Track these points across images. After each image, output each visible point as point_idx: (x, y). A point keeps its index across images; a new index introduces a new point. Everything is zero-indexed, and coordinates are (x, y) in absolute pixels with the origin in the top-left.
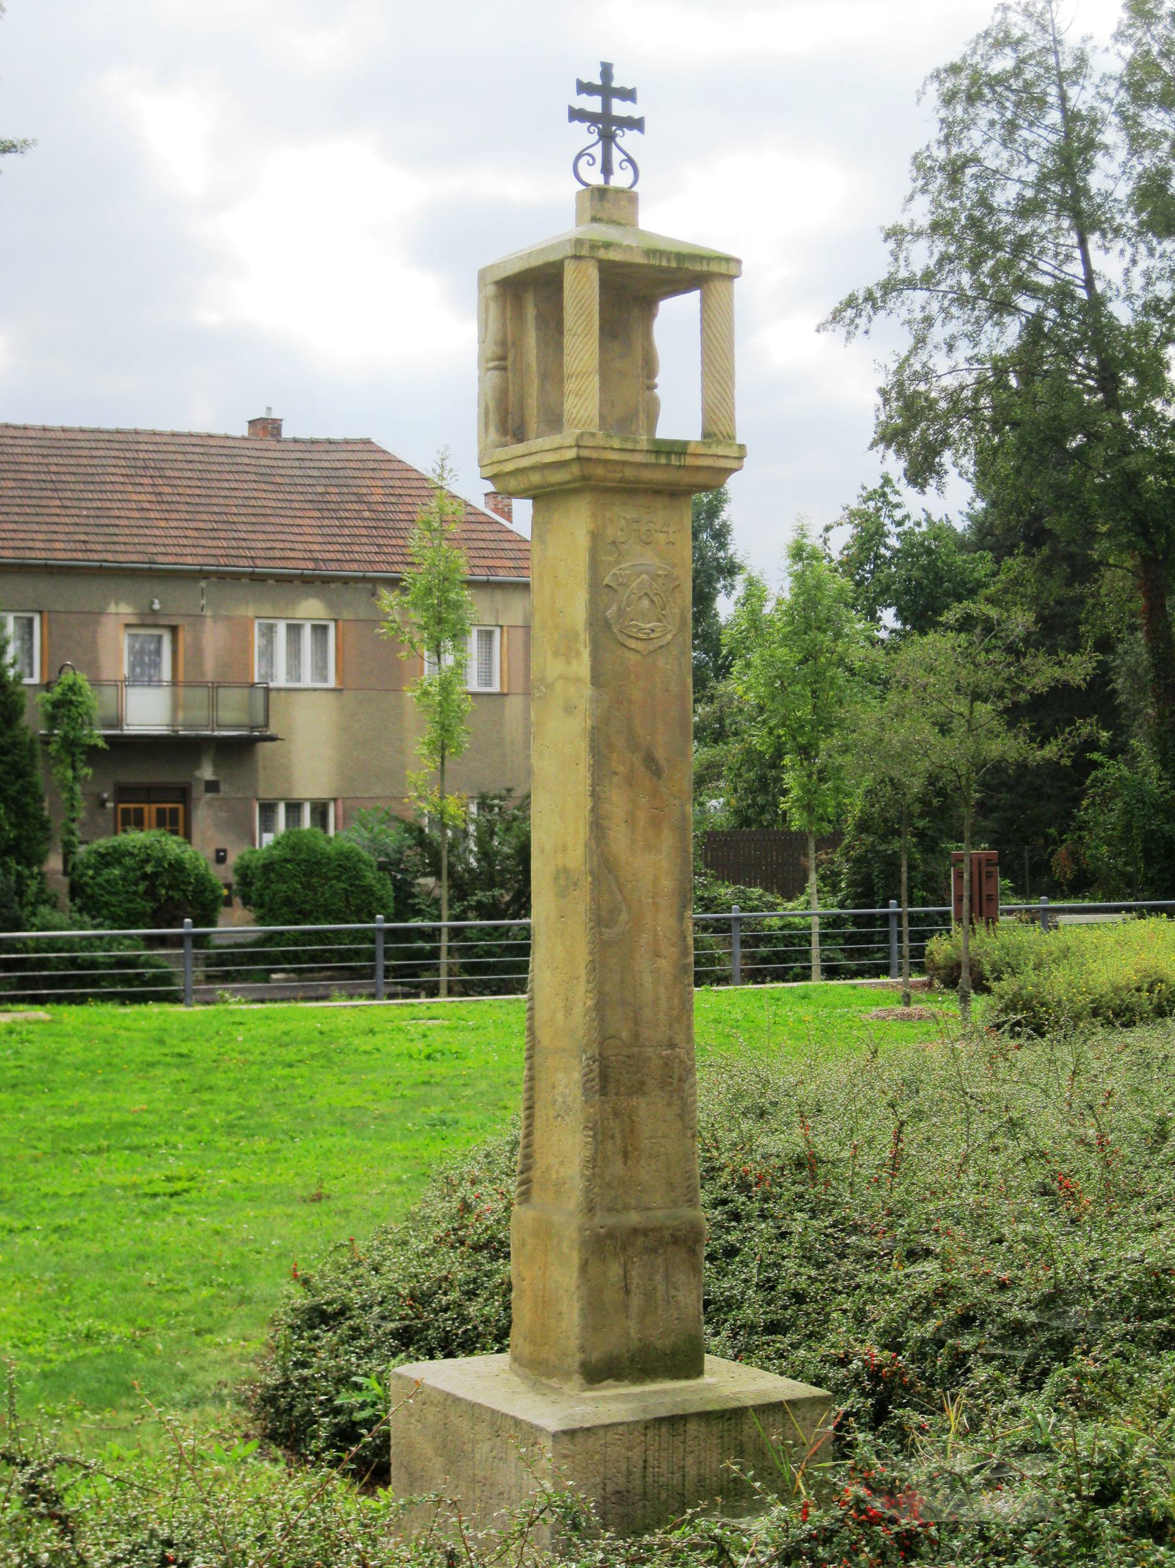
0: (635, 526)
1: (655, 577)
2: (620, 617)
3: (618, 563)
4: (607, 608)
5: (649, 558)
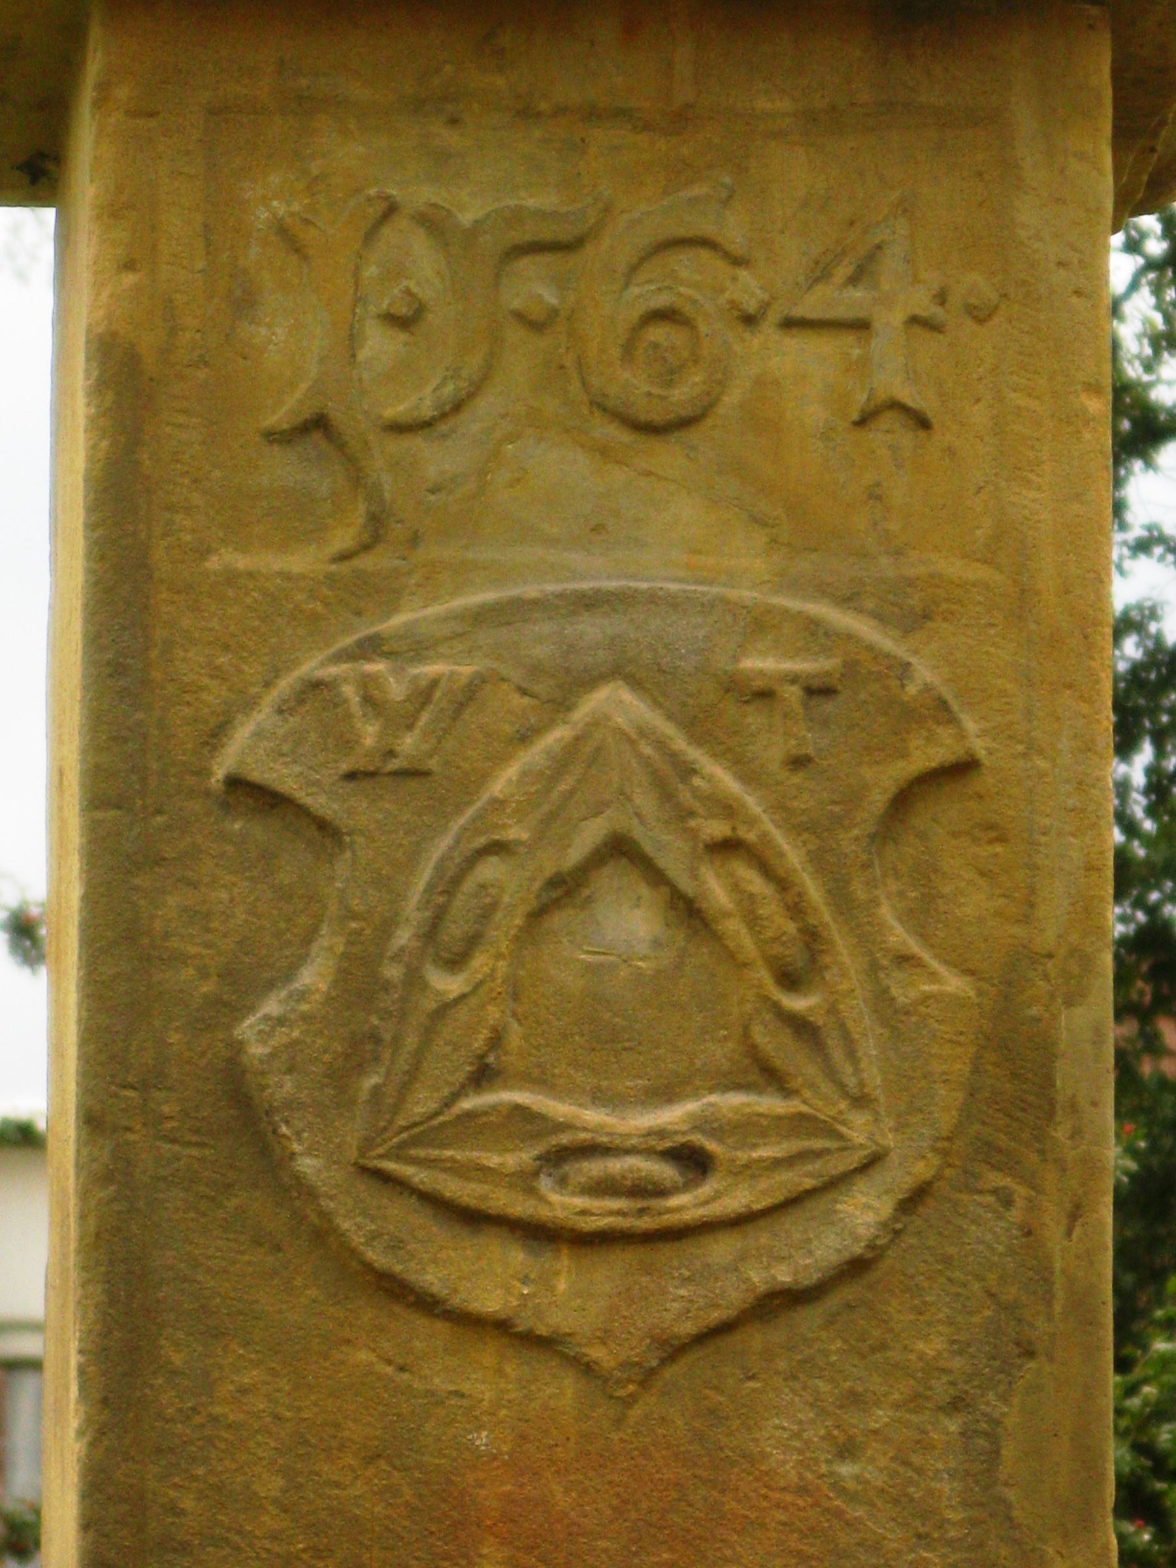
0: (534, 286)
1: (722, 706)
2: (362, 1050)
3: (355, 591)
4: (242, 983)
5: (684, 548)
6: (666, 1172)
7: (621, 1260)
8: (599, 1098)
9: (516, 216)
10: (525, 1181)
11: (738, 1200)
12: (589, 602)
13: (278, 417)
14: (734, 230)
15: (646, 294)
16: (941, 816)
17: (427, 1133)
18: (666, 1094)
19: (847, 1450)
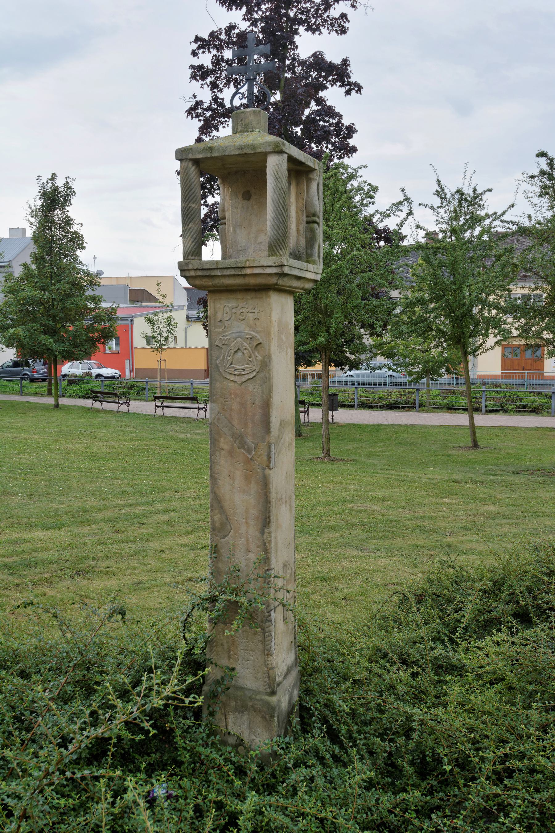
0: (234, 310)
4: (217, 358)
16: (259, 347)
17: (228, 368)
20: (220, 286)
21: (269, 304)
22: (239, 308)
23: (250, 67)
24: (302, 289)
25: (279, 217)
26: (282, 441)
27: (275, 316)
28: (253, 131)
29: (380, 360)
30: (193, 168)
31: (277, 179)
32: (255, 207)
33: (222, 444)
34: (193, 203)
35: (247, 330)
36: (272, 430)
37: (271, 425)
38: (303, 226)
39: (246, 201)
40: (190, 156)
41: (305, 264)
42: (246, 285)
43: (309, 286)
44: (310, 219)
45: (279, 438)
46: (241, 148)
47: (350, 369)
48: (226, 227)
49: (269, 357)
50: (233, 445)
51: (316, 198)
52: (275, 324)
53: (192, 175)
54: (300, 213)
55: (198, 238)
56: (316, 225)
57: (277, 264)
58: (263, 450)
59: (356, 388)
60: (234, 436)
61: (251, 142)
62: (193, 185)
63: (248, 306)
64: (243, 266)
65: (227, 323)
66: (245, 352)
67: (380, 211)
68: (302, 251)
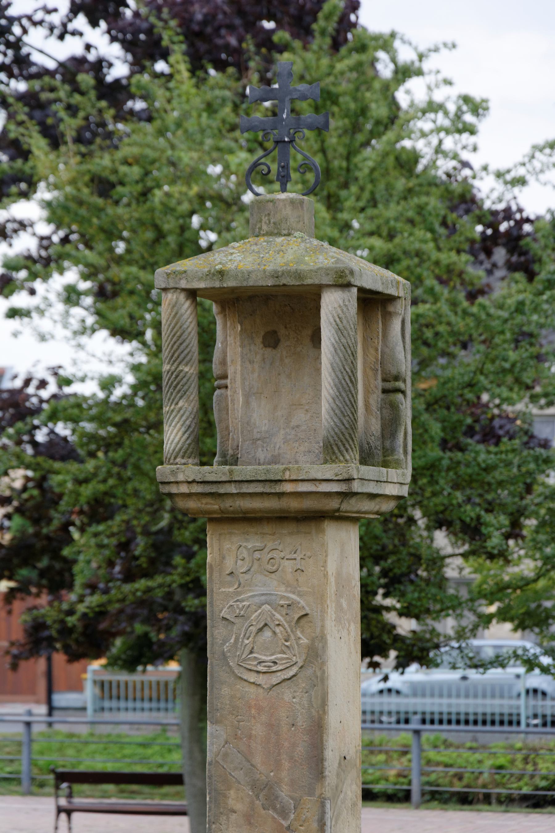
0: (257, 555)
4: (225, 642)
6: (272, 664)
7: (268, 675)
8: (265, 655)
9: (255, 547)
10: (256, 666)
11: (281, 668)
12: (263, 595)
13: (228, 572)
14: (280, 548)
15: (270, 556)
16: (303, 621)
17: (244, 660)
18: (272, 655)
19: (294, 698)
20: (233, 512)
21: (323, 545)
22: (266, 550)
23: (283, 120)
24: (377, 513)
25: (344, 395)
26: (342, 796)
27: (332, 567)
28: (289, 235)
29: (501, 636)
30: (188, 303)
31: (340, 331)
32: (286, 361)
33: (231, 802)
34: (186, 365)
35: (282, 591)
36: (327, 773)
37: (326, 764)
38: (376, 397)
39: (269, 350)
40: (183, 284)
41: (384, 470)
42: (281, 511)
43: (388, 506)
44: (389, 385)
45: (337, 790)
46: (276, 275)
47: (401, 665)
48: (229, 392)
49: (323, 638)
50: (252, 803)
51: (400, 348)
52: (332, 579)
53: (185, 316)
54: (371, 373)
55: (193, 425)
56: (400, 396)
57: (340, 477)
58: (310, 811)
59: (417, 732)
60: (254, 785)
61: (293, 267)
62: (186, 333)
63: (285, 549)
64: (279, 478)
65: (243, 578)
66: (278, 630)
67: (493, 167)
68: (375, 442)
